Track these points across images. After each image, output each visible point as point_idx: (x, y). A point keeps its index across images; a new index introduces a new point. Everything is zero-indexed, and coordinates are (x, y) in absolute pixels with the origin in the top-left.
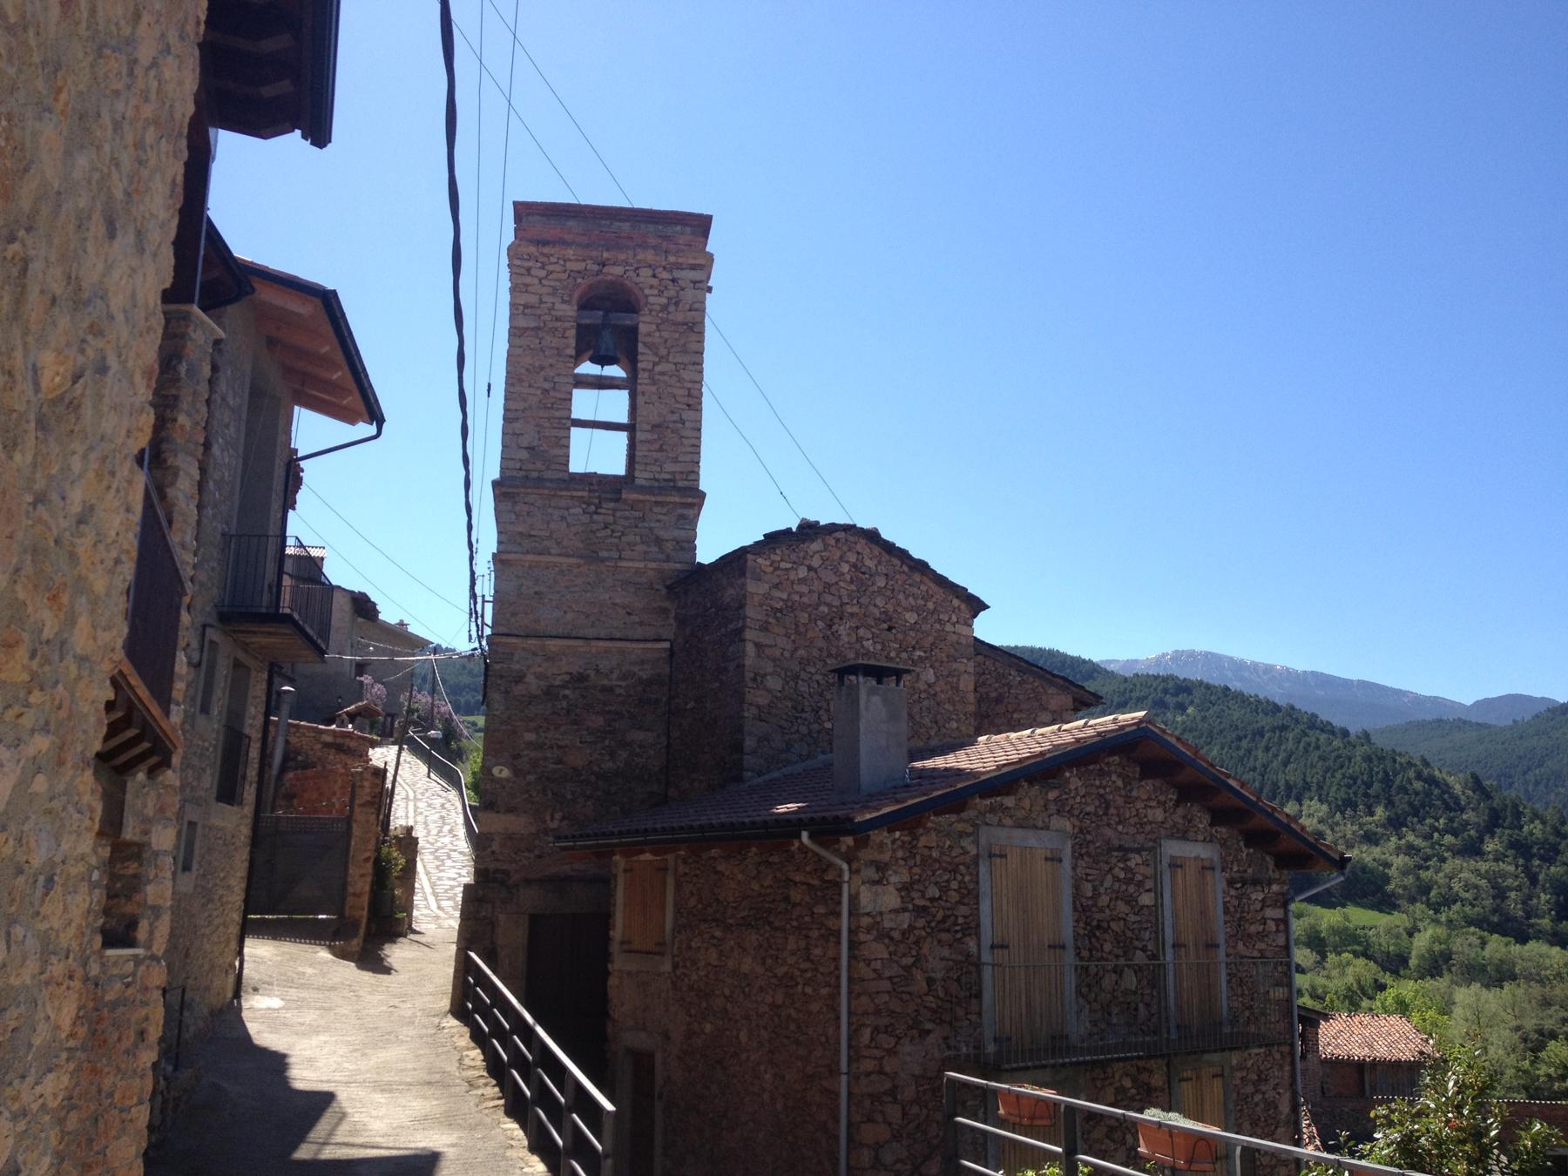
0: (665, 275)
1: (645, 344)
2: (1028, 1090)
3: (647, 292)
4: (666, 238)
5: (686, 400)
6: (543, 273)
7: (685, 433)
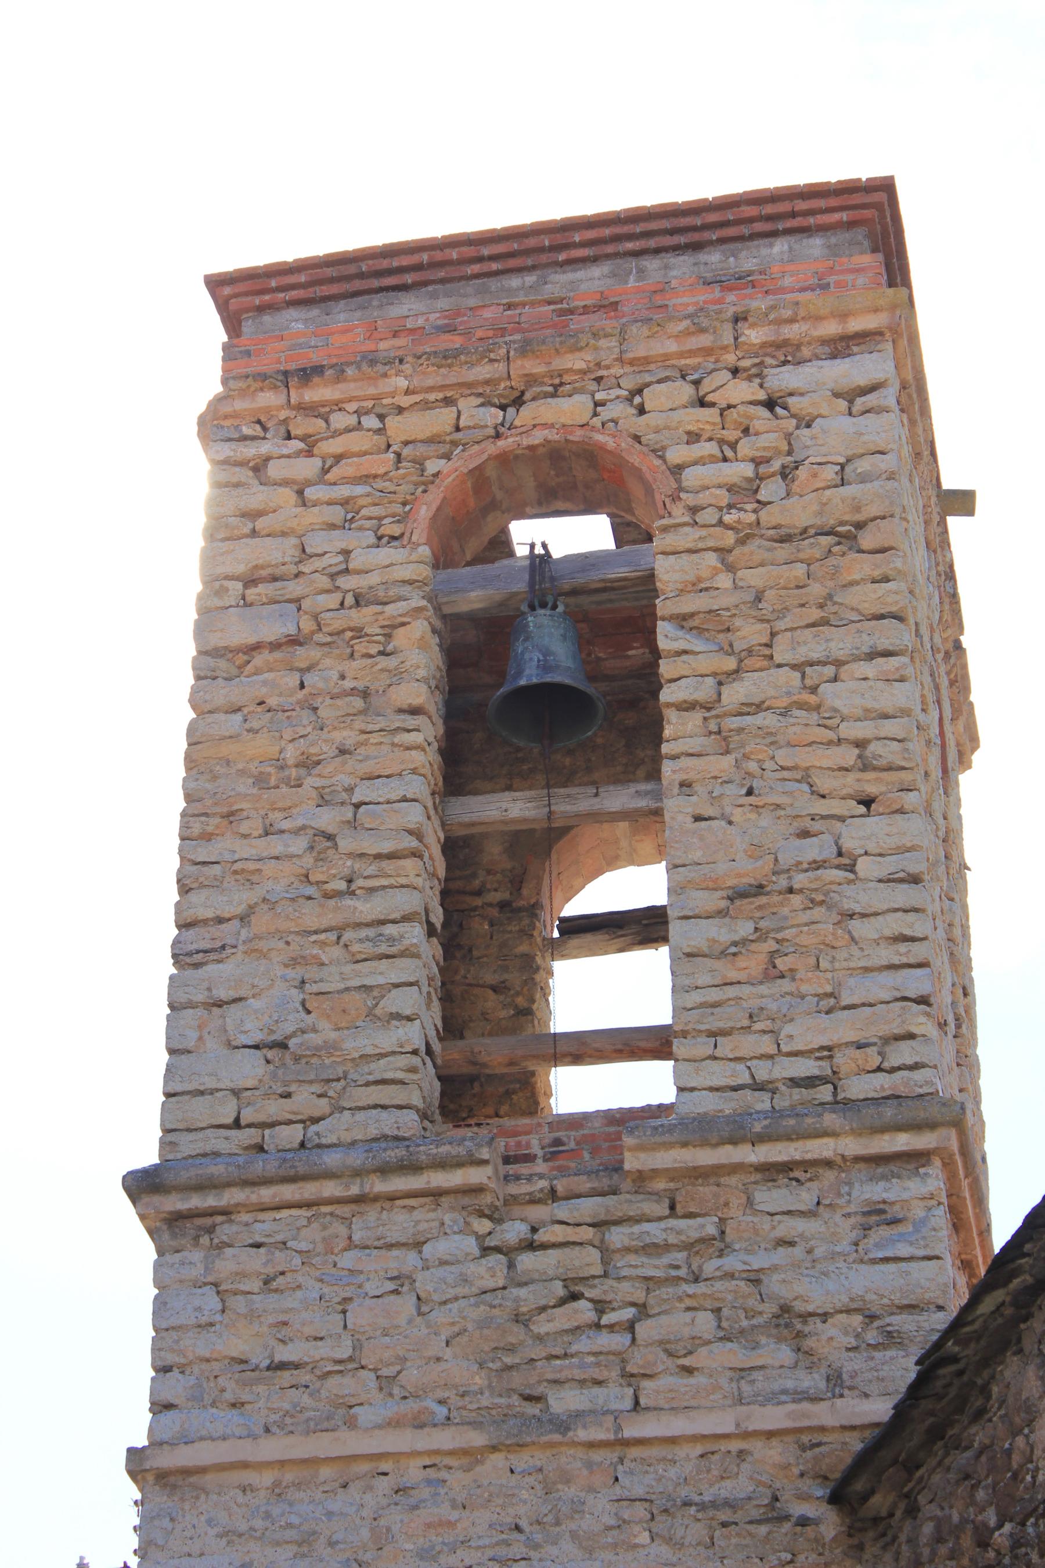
0: (741, 391)
1: (681, 620)
2: (971, 1214)
3: (676, 454)
4: (742, 281)
5: (851, 782)
6: (308, 468)
7: (855, 898)
